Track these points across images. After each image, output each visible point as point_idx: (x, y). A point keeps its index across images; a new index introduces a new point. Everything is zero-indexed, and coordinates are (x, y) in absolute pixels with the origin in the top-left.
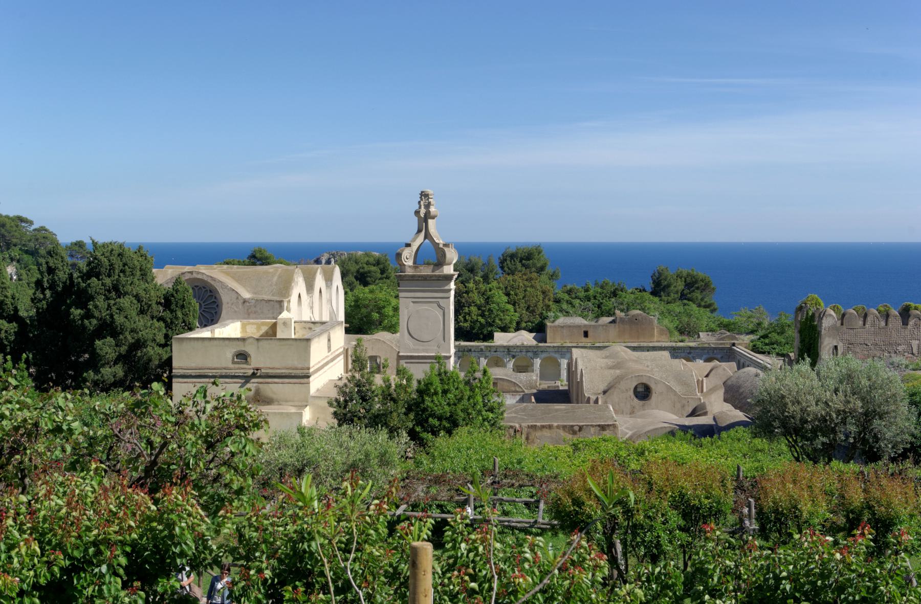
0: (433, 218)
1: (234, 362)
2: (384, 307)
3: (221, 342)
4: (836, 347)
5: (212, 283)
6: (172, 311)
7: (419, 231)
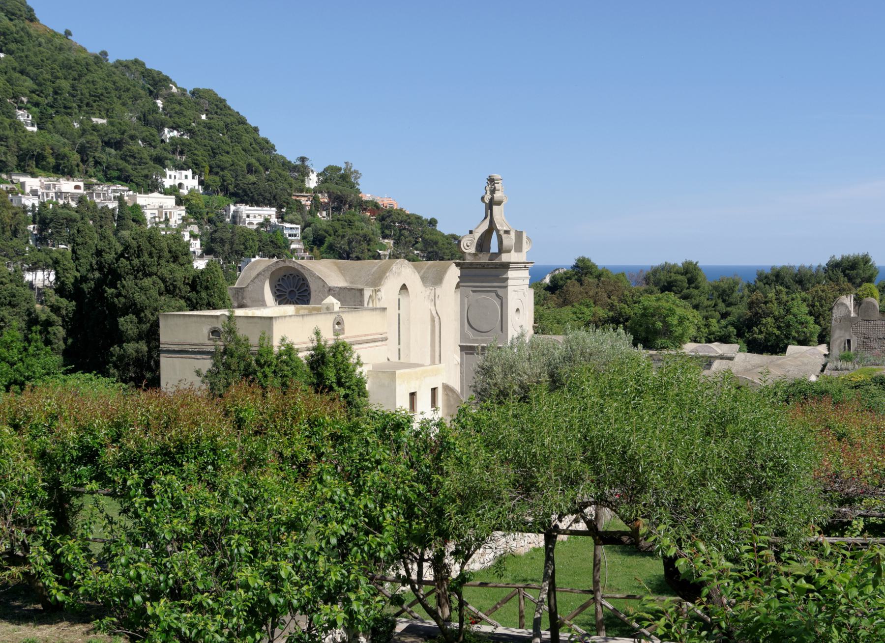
0: (499, 203)
1: (209, 339)
2: (668, 316)
3: (199, 318)
4: (849, 341)
5: (302, 271)
6: (197, 292)
7: (486, 218)
